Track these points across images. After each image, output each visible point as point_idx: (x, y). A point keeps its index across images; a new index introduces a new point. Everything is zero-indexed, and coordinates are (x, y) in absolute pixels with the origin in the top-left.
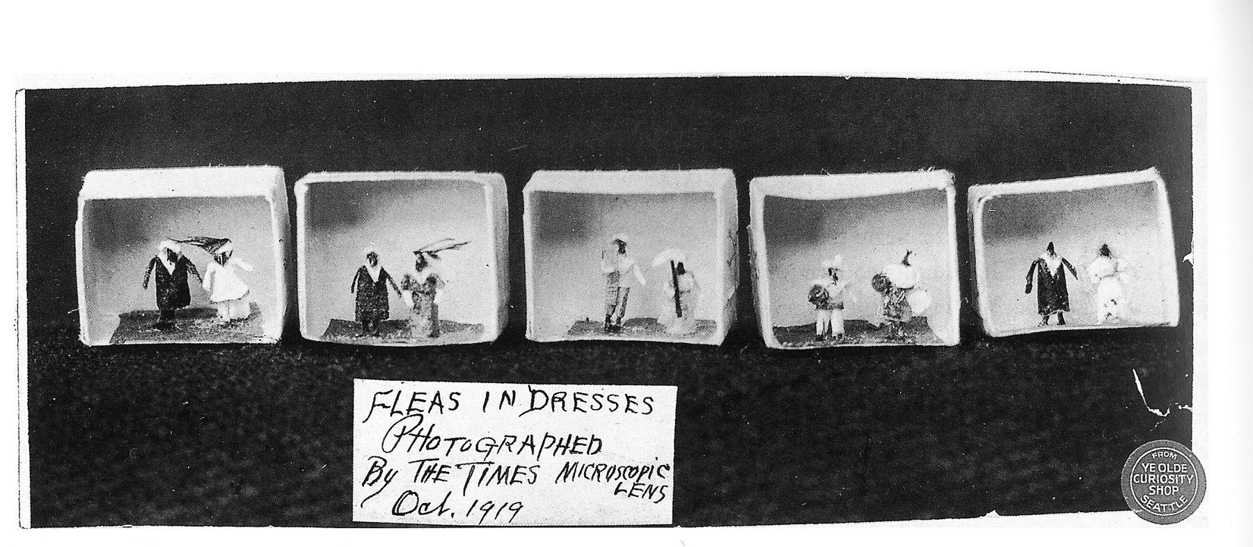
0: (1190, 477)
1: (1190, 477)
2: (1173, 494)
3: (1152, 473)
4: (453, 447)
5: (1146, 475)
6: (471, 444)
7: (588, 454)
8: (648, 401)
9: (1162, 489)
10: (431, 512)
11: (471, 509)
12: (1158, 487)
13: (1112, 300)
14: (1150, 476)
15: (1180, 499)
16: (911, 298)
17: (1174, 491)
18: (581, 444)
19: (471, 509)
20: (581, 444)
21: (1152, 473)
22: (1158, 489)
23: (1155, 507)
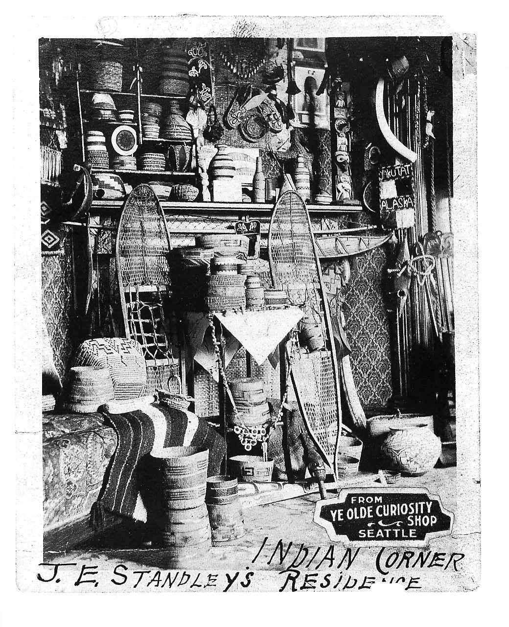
22: (416, 520)
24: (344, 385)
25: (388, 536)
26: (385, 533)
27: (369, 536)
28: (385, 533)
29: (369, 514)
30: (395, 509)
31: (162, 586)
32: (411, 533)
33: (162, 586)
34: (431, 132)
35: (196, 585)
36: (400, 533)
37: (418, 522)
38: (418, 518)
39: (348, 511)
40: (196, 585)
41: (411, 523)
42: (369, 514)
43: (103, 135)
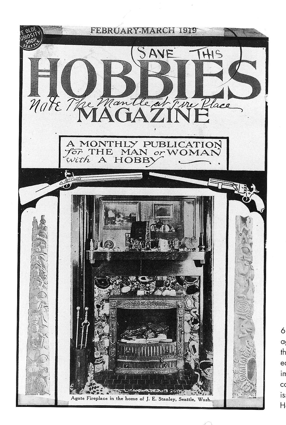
0: (39, 32)
1: (39, 32)
2: (35, 41)
3: (23, 35)
4: (200, 160)
5: (22, 37)
6: (152, 158)
7: (47, 103)
8: (283, 395)
9: (30, 41)
10: (229, 108)
11: (174, 105)
12: (28, 40)
13: (75, 158)
14: (23, 36)
15: (37, 41)
16: (109, 120)
17: (34, 40)
18: (186, 104)
19: (174, 105)
20: (186, 104)
21: (23, 35)
22: (29, 41)
23: (28, 47)
24: (85, 242)
25: (32, 47)
26: (31, 46)
27: (39, 42)
28: (31, 46)
29: (35, 30)
30: (25, 37)
31: (82, 150)
32: (38, 42)
33: (82, 150)
34: (201, 267)
35: (137, 118)
36: (35, 45)
37: (30, 42)
38: (29, 40)
39: (26, 31)
40: (137, 118)
41: (27, 43)
42: (35, 30)
43: (107, 117)
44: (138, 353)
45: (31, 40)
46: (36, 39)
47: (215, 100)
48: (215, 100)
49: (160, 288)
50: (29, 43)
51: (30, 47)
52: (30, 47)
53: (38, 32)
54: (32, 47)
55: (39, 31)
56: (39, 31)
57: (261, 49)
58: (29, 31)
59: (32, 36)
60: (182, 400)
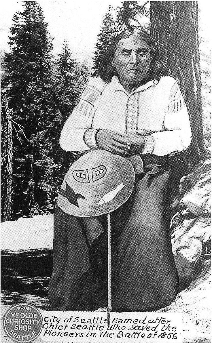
1: (38, 321)
2: (28, 330)
3: (16, 318)
12: (19, 326)
17: (28, 328)
23: (17, 337)
25: (23, 339)
32: (33, 334)
44: (14, 294)
45: (26, 329)
46: (31, 328)
47: (174, 328)
48: (174, 328)
49: (54, 163)
50: (19, 329)
51: (19, 338)
52: (19, 338)
53: (37, 320)
54: (23, 339)
55: (39, 320)
56: (39, 320)
57: (155, 154)
58: (26, 317)
59: (28, 321)
60: (46, 329)
